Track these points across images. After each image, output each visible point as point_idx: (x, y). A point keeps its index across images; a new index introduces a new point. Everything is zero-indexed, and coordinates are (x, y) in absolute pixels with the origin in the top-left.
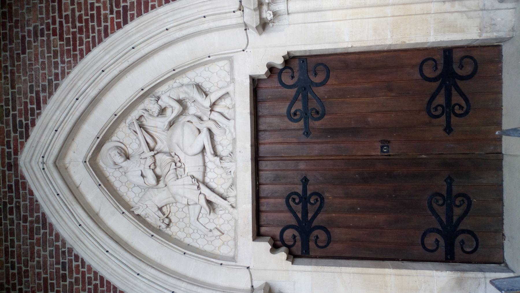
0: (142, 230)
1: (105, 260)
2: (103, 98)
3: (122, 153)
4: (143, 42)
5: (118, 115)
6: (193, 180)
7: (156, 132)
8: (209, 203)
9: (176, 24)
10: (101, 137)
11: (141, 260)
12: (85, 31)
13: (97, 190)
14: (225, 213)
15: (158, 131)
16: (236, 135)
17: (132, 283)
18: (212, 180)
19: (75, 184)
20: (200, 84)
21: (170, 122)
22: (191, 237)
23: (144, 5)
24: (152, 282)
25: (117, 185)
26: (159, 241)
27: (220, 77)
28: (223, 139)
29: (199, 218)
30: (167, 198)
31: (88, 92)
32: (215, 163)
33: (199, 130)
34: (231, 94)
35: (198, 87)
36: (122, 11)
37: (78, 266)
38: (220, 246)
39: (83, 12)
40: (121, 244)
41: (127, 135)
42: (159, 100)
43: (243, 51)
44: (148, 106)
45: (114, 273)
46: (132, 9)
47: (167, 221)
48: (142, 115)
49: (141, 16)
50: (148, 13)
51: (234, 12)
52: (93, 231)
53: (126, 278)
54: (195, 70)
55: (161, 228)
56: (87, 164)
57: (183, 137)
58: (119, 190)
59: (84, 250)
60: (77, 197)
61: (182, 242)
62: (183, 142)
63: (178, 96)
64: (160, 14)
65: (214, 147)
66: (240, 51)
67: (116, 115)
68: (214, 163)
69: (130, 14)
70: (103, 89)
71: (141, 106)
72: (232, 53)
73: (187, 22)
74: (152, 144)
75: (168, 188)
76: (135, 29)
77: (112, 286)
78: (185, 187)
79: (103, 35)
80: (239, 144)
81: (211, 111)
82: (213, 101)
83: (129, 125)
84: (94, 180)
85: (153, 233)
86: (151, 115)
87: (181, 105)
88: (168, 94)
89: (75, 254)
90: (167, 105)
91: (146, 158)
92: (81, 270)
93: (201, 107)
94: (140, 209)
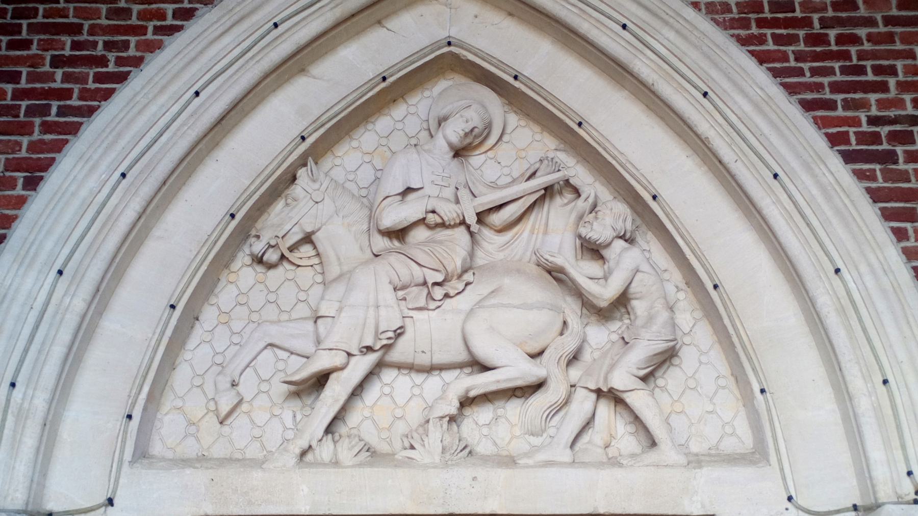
0: (252, 188)
1: (174, 88)
2: (627, 92)
3: (472, 137)
4: (795, 203)
5: (581, 132)
6: (391, 334)
7: (532, 232)
8: (321, 380)
9: (856, 296)
10: (517, 84)
11: (164, 183)
12: (815, 51)
13: (371, 71)
14: (285, 428)
15: (535, 236)
16: (527, 466)
17: (101, 157)
18: (387, 390)
19: (387, 16)
20: (676, 361)
21: (562, 270)
22: (220, 327)
23: (904, 208)
24: (99, 213)
25: (383, 123)
26: (215, 234)
27: (699, 421)
28: (513, 426)
29: (275, 349)
30: (339, 259)
31: (645, 55)
32: (440, 401)
33: (541, 353)
34: (652, 456)
35: (670, 353)
36: (880, 148)
37: (163, 17)
38: (185, 414)
39: (867, 46)
40: (216, 129)
41: (523, 154)
42: (626, 241)
43: (790, 499)
44: (608, 212)
45: (136, 110)
46: (888, 176)
47: (272, 256)
48: (579, 196)
49: (871, 201)
50: (883, 220)
51: (910, 473)
52: (257, 58)
53: (115, 141)
54: (717, 346)
55: (253, 240)
56: (443, 47)
57: (518, 307)
58: (367, 130)
59: (206, 34)
60: (354, 20)
61: (206, 299)
62: (503, 305)
63: (638, 296)
64: (883, 253)
65: (487, 398)
66: (787, 488)
67: (580, 124)
68: (441, 398)
69: (874, 170)
70: (653, 93)
71: (604, 193)
72: (780, 461)
73: (864, 330)
74: (497, 219)
75: (366, 263)
76: (833, 181)
77: (96, 103)
78: (371, 312)
79: (809, 96)
80: (500, 475)
81: (599, 392)
82: (629, 398)
83: (552, 159)
84: (399, 65)
85: (239, 217)
86: (581, 217)
87: (612, 303)
88: (645, 267)
89: (196, 9)
90: (612, 263)
91: (457, 202)
92: (151, 25)
93: (608, 362)
94: (310, 183)
